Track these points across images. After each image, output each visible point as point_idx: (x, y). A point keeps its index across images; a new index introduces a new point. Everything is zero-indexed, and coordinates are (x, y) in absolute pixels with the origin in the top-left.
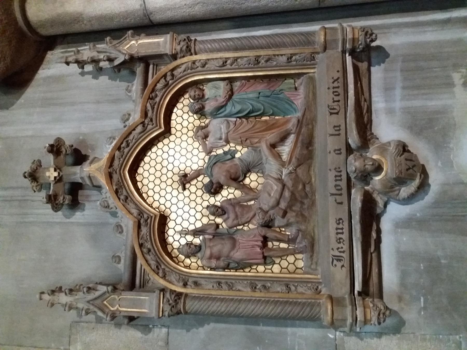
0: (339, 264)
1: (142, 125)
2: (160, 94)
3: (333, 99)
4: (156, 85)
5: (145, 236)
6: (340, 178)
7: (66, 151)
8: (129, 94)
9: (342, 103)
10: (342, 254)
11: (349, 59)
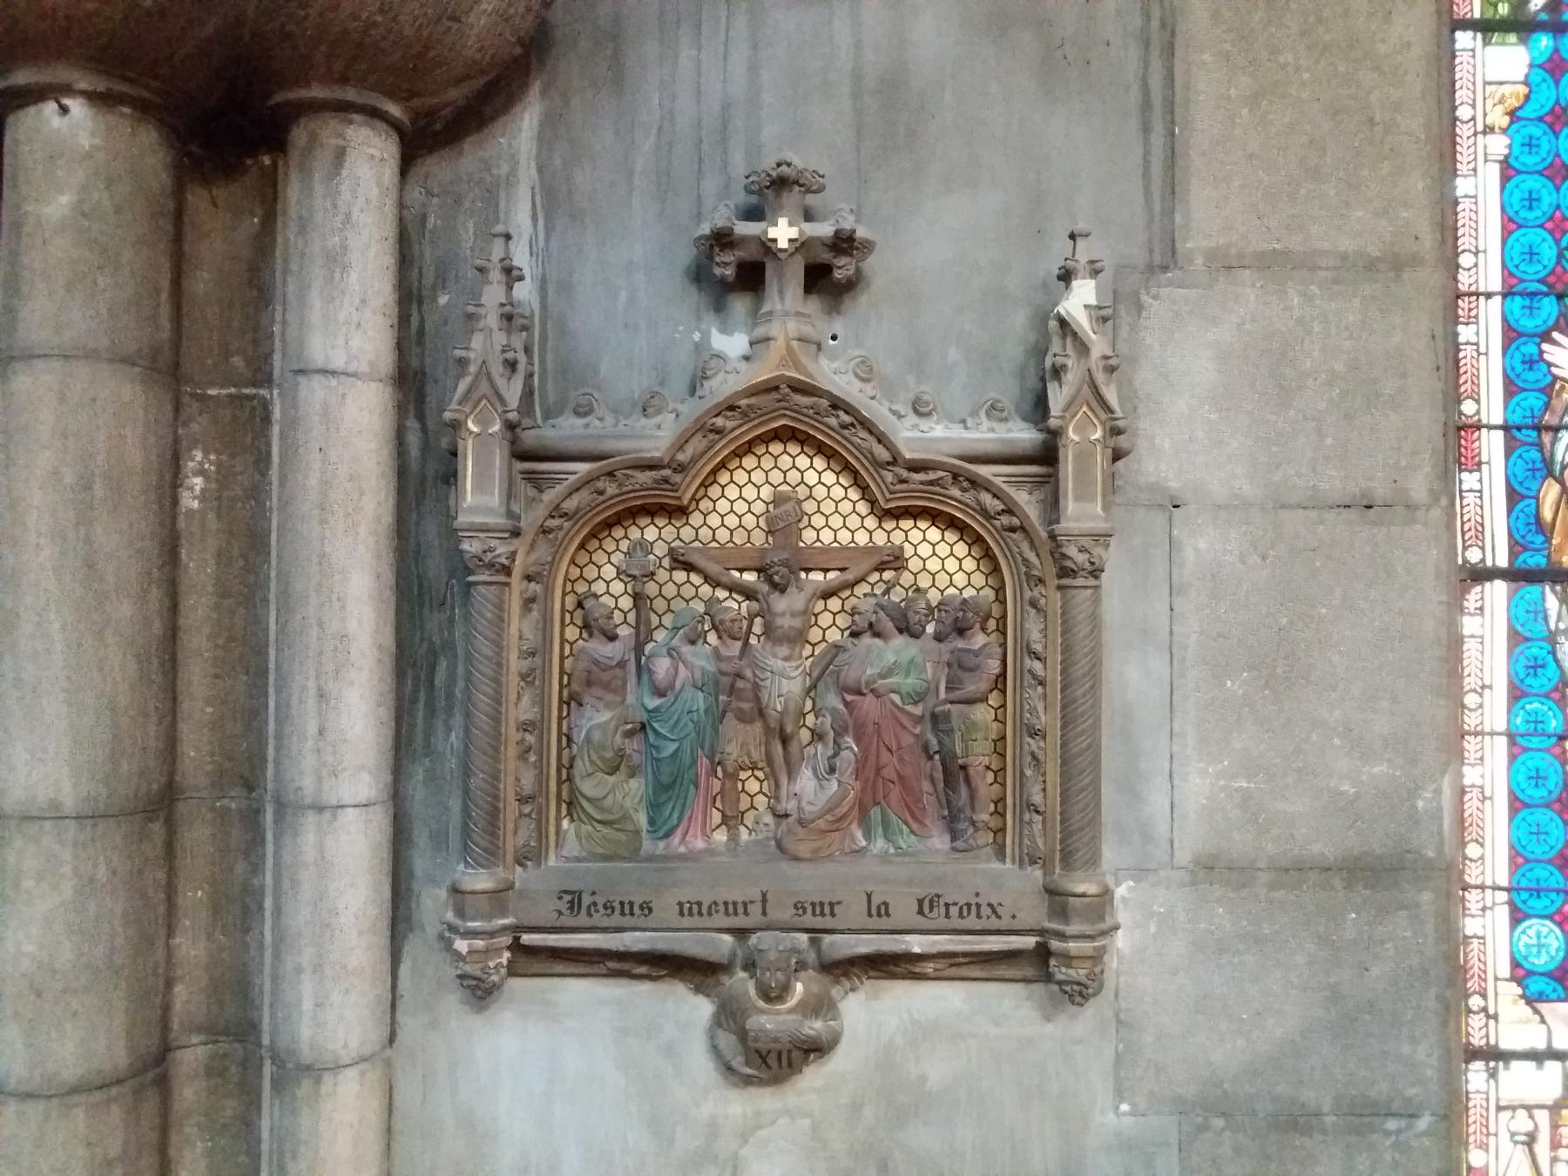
0: (563, 905)
1: (891, 460)
2: (968, 497)
3: (955, 904)
4: (988, 490)
5: (633, 481)
6: (818, 912)
7: (840, 268)
8: (983, 411)
9: (942, 923)
10: (584, 911)
11: (1030, 942)
